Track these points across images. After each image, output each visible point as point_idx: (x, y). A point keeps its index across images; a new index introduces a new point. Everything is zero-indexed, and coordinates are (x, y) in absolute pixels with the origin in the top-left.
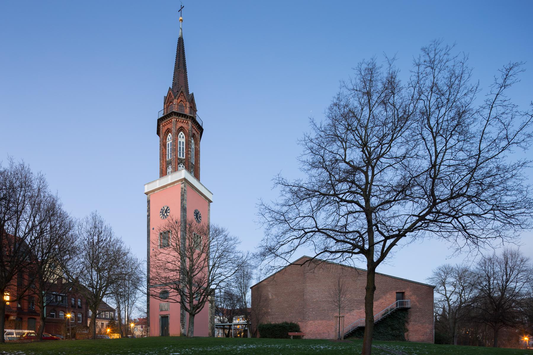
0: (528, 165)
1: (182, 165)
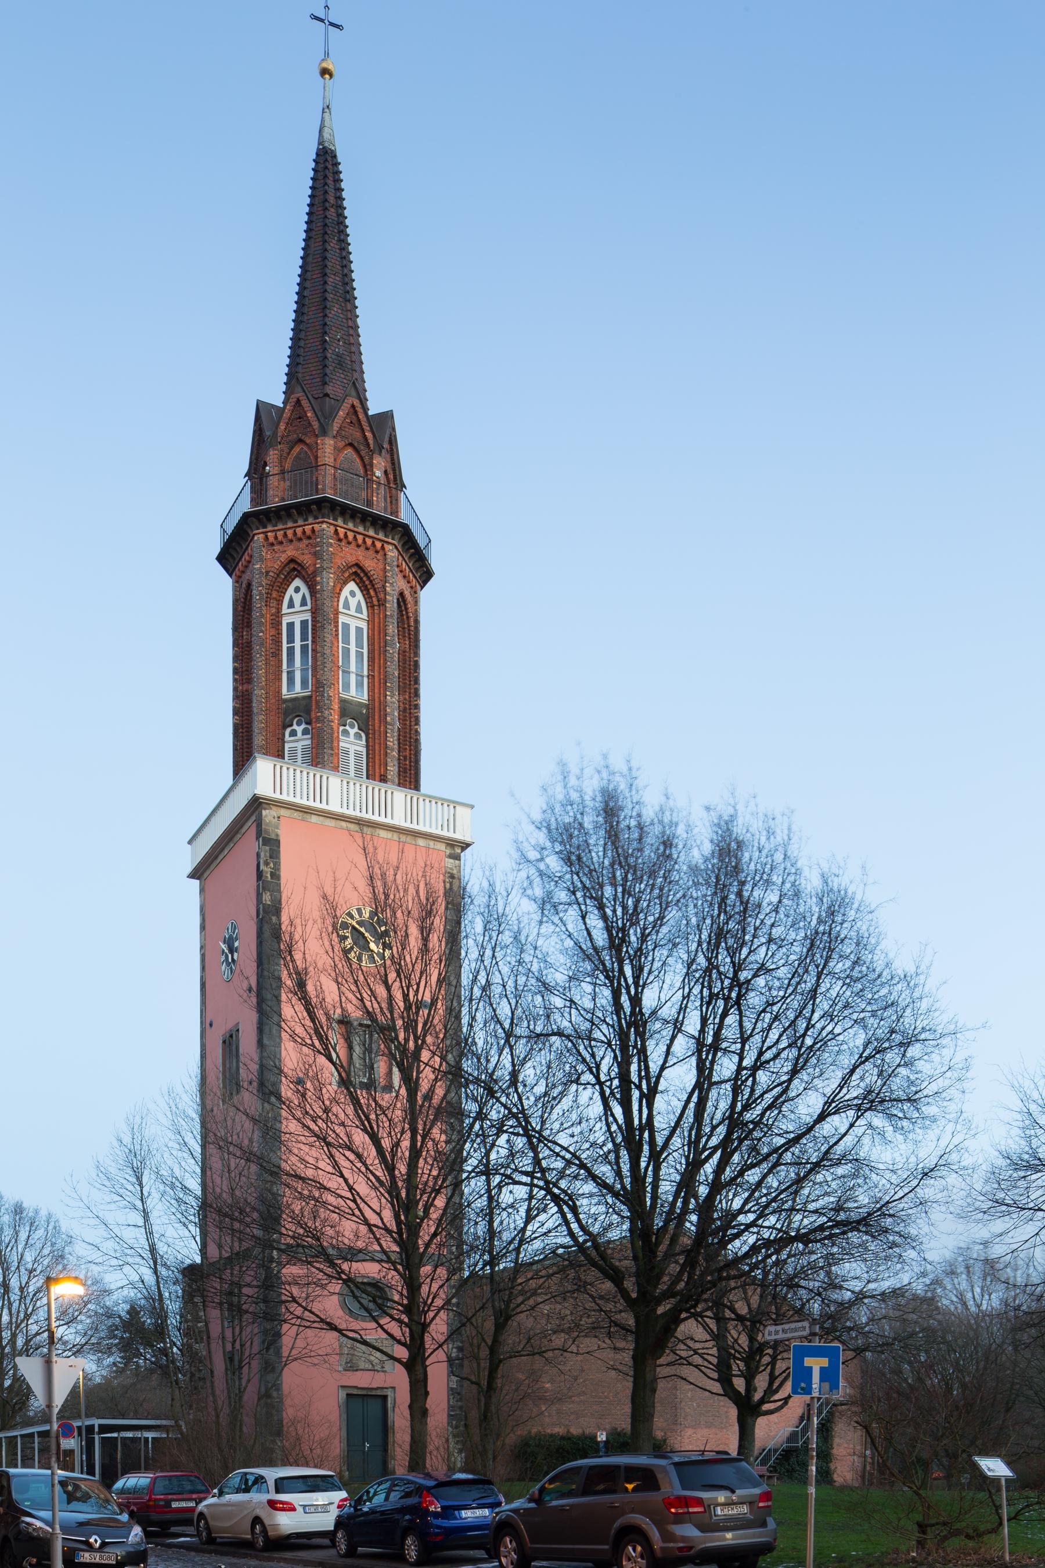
0: (329, 891)
1: (356, 730)
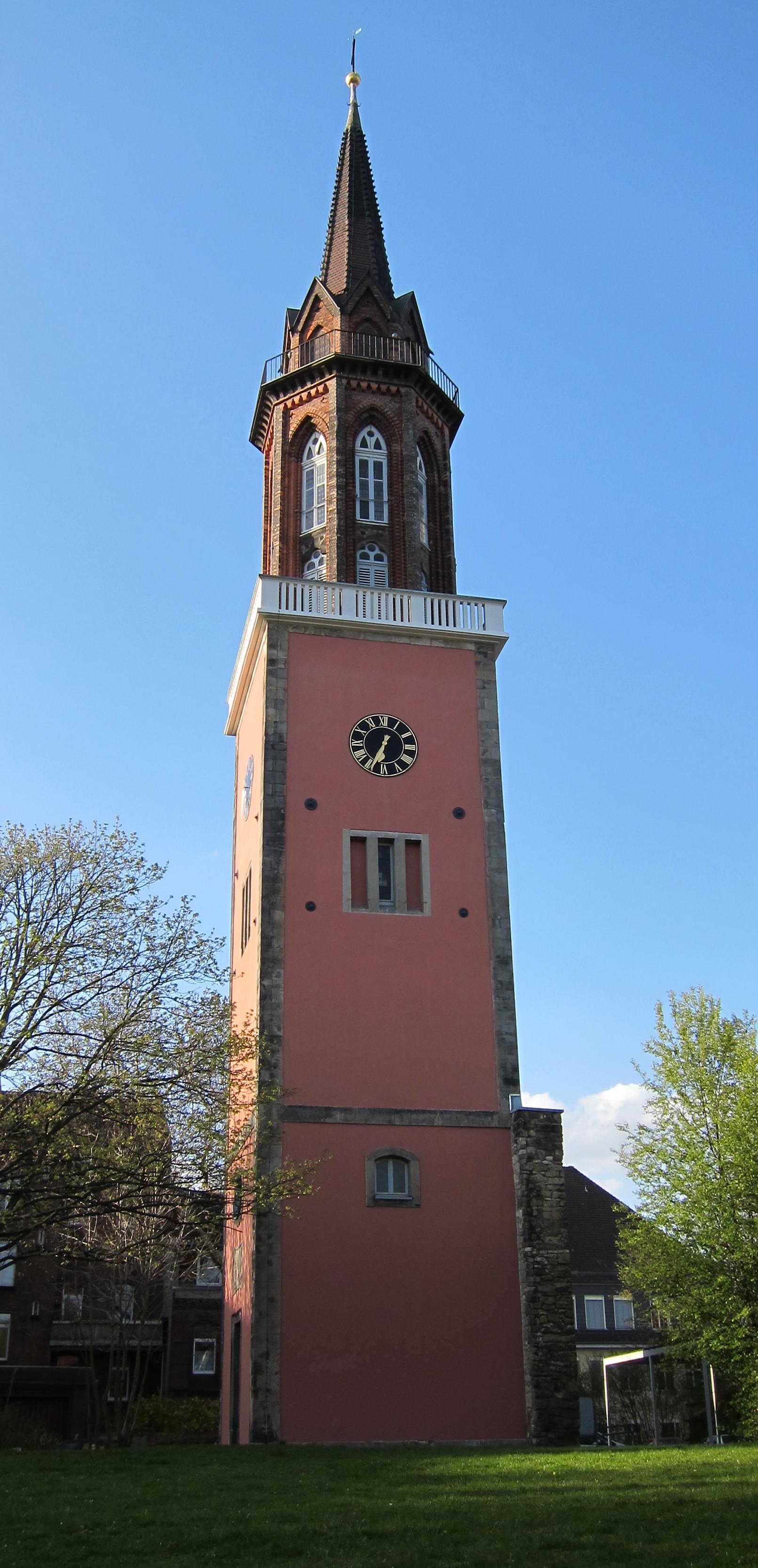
1: (377, 551)
